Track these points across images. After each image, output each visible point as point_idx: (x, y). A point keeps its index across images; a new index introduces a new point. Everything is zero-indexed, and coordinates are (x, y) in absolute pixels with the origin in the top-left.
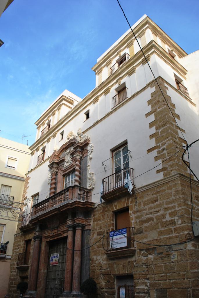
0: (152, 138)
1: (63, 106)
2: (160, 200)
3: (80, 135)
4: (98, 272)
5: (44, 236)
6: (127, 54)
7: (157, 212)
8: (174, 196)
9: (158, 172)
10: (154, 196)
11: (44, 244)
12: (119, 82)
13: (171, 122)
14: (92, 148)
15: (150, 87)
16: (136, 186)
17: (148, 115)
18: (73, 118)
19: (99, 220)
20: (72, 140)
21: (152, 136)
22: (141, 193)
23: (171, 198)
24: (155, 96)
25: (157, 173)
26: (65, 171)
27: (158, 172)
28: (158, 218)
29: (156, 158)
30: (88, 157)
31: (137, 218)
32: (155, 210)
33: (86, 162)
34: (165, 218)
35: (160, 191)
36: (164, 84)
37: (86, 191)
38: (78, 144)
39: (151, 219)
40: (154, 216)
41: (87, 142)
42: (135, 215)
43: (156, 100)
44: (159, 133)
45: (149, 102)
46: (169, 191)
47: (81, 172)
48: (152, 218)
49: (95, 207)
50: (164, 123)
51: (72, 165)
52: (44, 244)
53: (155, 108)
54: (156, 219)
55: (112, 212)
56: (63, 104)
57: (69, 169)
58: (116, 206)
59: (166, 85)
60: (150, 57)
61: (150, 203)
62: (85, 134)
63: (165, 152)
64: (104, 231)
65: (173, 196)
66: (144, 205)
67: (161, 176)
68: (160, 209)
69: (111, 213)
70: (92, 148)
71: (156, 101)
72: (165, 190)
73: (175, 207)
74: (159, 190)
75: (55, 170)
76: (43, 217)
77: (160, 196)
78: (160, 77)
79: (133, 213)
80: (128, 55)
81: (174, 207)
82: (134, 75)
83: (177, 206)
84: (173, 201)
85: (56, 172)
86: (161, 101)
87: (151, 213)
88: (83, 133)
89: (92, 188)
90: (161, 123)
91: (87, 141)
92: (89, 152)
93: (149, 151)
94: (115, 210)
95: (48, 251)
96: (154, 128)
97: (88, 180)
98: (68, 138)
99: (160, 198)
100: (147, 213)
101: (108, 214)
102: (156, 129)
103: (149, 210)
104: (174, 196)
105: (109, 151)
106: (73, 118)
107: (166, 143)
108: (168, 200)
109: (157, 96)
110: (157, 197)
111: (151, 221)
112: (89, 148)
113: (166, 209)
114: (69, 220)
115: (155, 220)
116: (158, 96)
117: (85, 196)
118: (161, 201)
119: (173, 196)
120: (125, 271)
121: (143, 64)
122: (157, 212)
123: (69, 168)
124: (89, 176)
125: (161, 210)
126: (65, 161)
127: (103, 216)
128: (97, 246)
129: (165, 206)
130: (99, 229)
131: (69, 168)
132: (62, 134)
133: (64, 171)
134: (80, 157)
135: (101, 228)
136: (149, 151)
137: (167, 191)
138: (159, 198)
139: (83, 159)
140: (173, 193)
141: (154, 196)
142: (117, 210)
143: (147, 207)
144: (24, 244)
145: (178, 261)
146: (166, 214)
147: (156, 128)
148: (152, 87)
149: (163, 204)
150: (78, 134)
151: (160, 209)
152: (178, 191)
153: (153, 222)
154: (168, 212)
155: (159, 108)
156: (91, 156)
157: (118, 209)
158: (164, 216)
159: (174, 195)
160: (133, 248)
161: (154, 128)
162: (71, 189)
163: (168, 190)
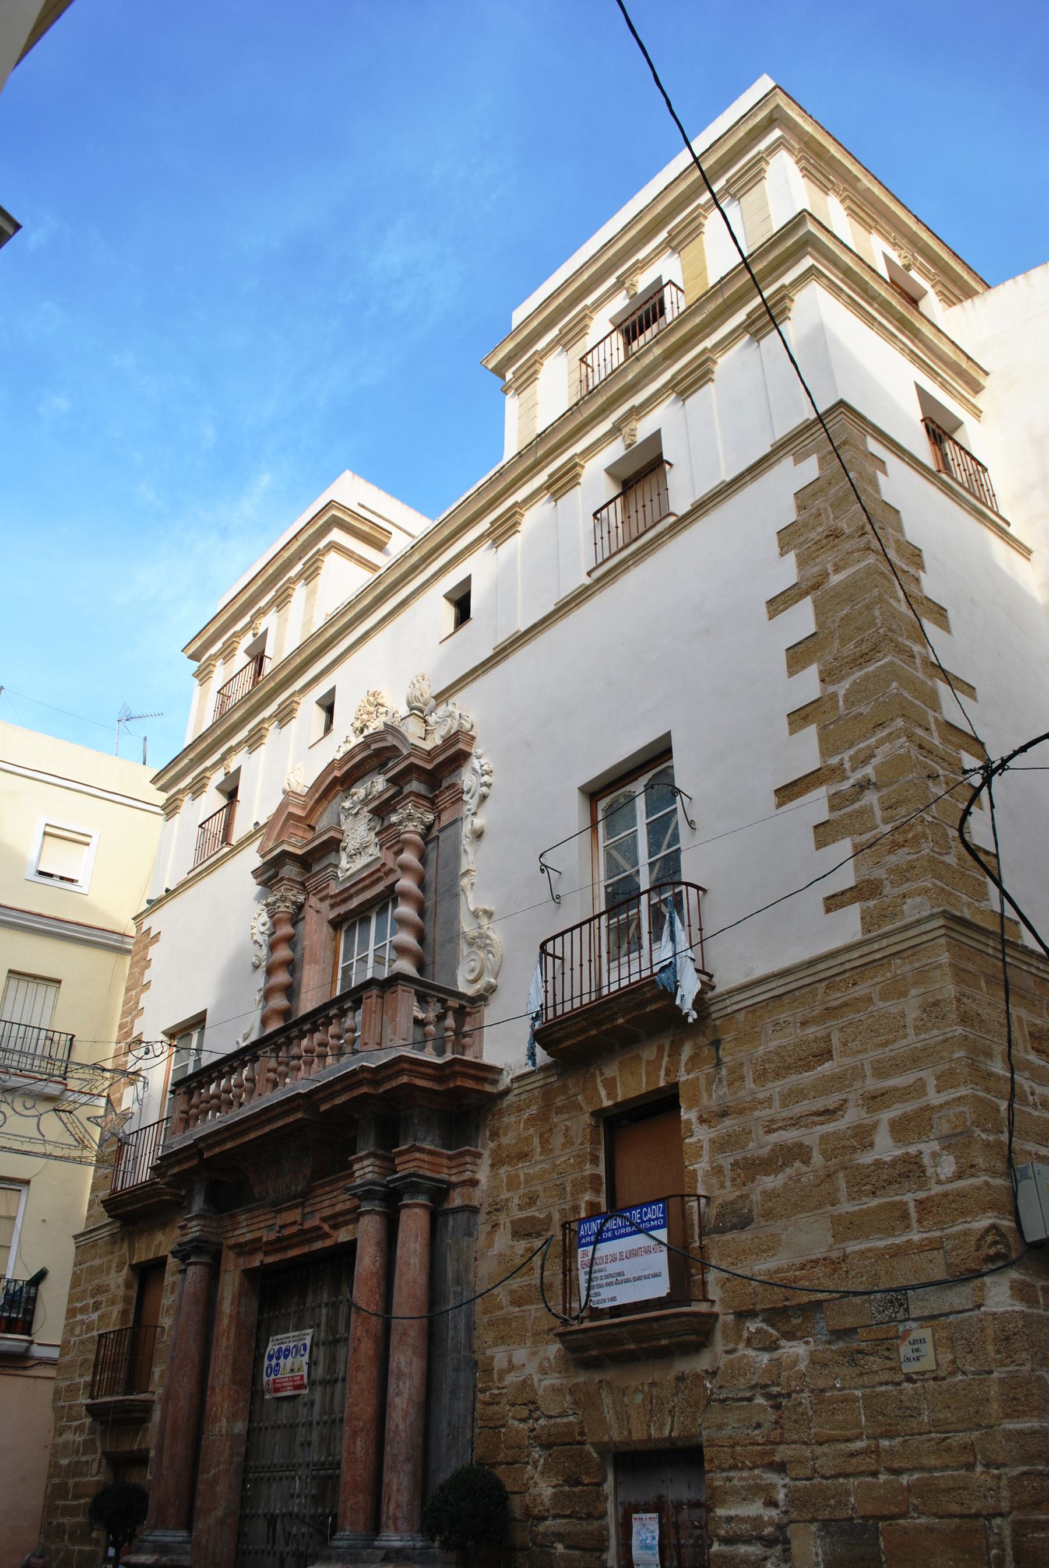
0: (802, 727)
3: (422, 712)
5: (232, 1241)
6: (670, 282)
7: (829, 1113)
9: (834, 902)
10: (811, 1031)
12: (626, 430)
13: (900, 639)
14: (486, 778)
17: (778, 604)
19: (523, 1156)
20: (377, 736)
21: (799, 718)
22: (741, 1016)
23: (904, 1042)
24: (819, 503)
25: (828, 910)
26: (345, 901)
27: (834, 902)
28: (833, 1147)
30: (466, 828)
31: (721, 1145)
32: (820, 1104)
34: (872, 1145)
37: (453, 1003)
38: (410, 755)
39: (799, 1153)
40: (811, 1136)
44: (841, 703)
45: (787, 538)
46: (892, 1007)
47: (429, 904)
48: (800, 1145)
49: (501, 1087)
50: (864, 648)
51: (378, 870)
53: (818, 568)
54: (823, 1152)
55: (593, 1114)
56: (333, 546)
58: (610, 1085)
59: (874, 446)
60: (792, 300)
61: (788, 1068)
62: (450, 708)
64: (549, 1217)
65: (911, 1031)
66: (762, 1077)
69: (586, 1118)
72: (869, 1000)
73: (924, 1087)
74: (837, 998)
77: (841, 1030)
79: (702, 1120)
80: (674, 289)
81: (918, 1089)
83: (931, 1083)
84: (915, 1059)
85: (294, 903)
86: (847, 531)
87: (795, 1122)
88: (436, 698)
90: (851, 646)
91: (457, 742)
93: (787, 793)
94: (607, 1103)
97: (464, 949)
98: (358, 724)
99: (845, 1044)
102: (822, 681)
103: (784, 1105)
107: (876, 751)
110: (828, 1038)
111: (797, 1164)
112: (467, 779)
113: (875, 1100)
114: (361, 1159)
115: (817, 1159)
116: (832, 505)
117: (446, 1030)
118: (846, 1060)
119: (911, 1031)
120: (661, 1428)
122: (829, 1113)
125: (850, 1104)
127: (541, 1135)
128: (512, 1292)
129: (872, 1084)
130: (521, 1207)
133: (338, 899)
136: (787, 793)
137: (881, 1004)
138: (835, 1042)
143: (776, 1087)
144: (128, 1285)
145: (941, 1374)
146: (874, 1127)
147: (821, 672)
149: (857, 1073)
150: (409, 703)
153: (804, 1169)
154: (886, 1116)
155: (837, 569)
156: (478, 822)
158: (863, 1136)
159: (916, 1028)
160: (703, 1307)
163: (885, 996)
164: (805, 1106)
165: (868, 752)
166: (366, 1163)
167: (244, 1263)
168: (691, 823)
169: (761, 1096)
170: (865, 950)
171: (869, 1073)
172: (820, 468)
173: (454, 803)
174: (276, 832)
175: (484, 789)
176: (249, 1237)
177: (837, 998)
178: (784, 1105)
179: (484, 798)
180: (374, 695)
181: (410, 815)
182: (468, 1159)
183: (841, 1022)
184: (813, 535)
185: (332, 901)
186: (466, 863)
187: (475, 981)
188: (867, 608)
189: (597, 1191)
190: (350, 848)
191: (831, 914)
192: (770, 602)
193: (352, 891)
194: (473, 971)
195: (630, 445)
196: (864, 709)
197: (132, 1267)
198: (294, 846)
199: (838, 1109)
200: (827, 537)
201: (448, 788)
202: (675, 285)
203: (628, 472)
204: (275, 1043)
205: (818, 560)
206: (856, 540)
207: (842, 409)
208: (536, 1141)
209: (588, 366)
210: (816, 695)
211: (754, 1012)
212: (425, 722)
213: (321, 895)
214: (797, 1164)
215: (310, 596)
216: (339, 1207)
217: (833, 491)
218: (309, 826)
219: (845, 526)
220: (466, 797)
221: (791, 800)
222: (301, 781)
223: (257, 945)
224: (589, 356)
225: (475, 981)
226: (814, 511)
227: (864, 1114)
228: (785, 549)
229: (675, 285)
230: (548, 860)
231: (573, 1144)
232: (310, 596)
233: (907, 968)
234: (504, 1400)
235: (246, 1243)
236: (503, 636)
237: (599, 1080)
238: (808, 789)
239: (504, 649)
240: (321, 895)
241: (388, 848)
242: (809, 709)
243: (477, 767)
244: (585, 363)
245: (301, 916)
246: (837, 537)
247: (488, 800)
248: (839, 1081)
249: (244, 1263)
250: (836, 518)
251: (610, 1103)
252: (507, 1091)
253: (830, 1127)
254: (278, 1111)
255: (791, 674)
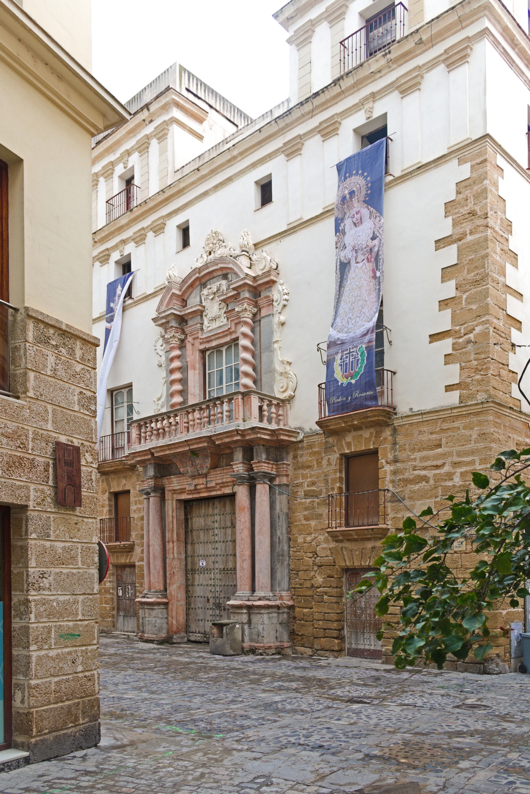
0: (445, 309)
1: (175, 129)
2: (446, 447)
3: (248, 253)
4: (308, 561)
5: (171, 488)
6: (401, 3)
7: (437, 467)
8: (475, 442)
9: (449, 388)
10: (434, 436)
11: (171, 506)
12: (366, 107)
13: (494, 275)
14: (286, 297)
15: (457, 161)
16: (397, 410)
17: (440, 243)
18: (216, 188)
19: (309, 467)
20: (222, 259)
21: (444, 304)
22: (407, 426)
23: (470, 446)
24: (467, 193)
25: (446, 391)
26: (208, 342)
27: (449, 388)
28: (438, 479)
29: (448, 359)
30: (276, 319)
31: (395, 473)
32: (435, 463)
33: (271, 333)
34: (452, 479)
35: (447, 429)
36: (495, 158)
37: (275, 402)
38: (245, 278)
39: (425, 479)
40: (430, 473)
41: (273, 278)
42: (392, 468)
43: (467, 205)
44: (464, 302)
45: (449, 207)
46: (467, 432)
47: (257, 352)
48: (426, 476)
49: (299, 439)
50: (478, 278)
51: (227, 331)
52: (171, 506)
53: (462, 230)
54: (434, 480)
55: (340, 454)
56: (174, 120)
57: (219, 338)
58: (349, 445)
59: (501, 161)
60: (471, 49)
61: (424, 449)
62: (264, 254)
63: (470, 347)
64: (321, 490)
65: (472, 442)
66: (413, 450)
67: (454, 398)
68: (445, 463)
69: (338, 455)
70: (286, 297)
71: (466, 208)
72: (458, 428)
73: (475, 462)
74: (445, 426)
75: (177, 335)
76: (166, 450)
77: (446, 438)
78: (487, 136)
79: (387, 463)
80: (402, 8)
81: (473, 462)
82: (414, 98)
83: (478, 462)
84: (472, 453)
85: (179, 339)
86: (479, 213)
87: (425, 468)
88: (255, 245)
89: (289, 397)
90: (472, 274)
91: (270, 275)
92: (277, 307)
93: (434, 337)
94: (347, 451)
95: (183, 517)
96: (452, 283)
97: (278, 377)
98: (208, 249)
99: (447, 443)
100: (415, 467)
101: (329, 459)
102: (457, 289)
103: (421, 462)
104: (475, 442)
105: (253, 184)
106: (216, 188)
107: (476, 328)
108: (460, 448)
109: (471, 195)
110: (441, 440)
111: (424, 482)
112: (275, 294)
113: (455, 464)
114: (236, 464)
115: (432, 482)
116: (473, 196)
117: (272, 413)
118: (446, 449)
119: (472, 442)
120: (365, 562)
121: (448, 66)
122: (437, 467)
123: (217, 336)
124: (279, 368)
125: (447, 464)
126: (206, 316)
127: (317, 460)
128: (304, 515)
129: (456, 459)
130: (308, 486)
131: (217, 336)
132: (185, 231)
133: (205, 340)
134: (251, 316)
135: (313, 484)
136: (434, 337)
137: (463, 431)
138: (444, 441)
139: (260, 321)
140: (475, 436)
141: (435, 436)
142: (351, 452)
143: (418, 455)
144: (110, 500)
145: (467, 551)
146: (454, 473)
147: (457, 284)
148: (461, 162)
149: (450, 454)
150: (241, 247)
151: (445, 463)
152: (484, 434)
153: (426, 484)
154: (459, 470)
155: (471, 233)
156: (282, 318)
157: (353, 450)
158: (450, 476)
159: (475, 441)
160: (384, 526)
161: (452, 283)
162: (240, 397)
163: (465, 428)
164: (429, 463)
165: (472, 327)
166: (239, 466)
167: (177, 497)
168: (390, 342)
169: (412, 457)
170: (460, 410)
171: (455, 454)
172: (471, 172)
173: (268, 305)
174: (166, 302)
175: (285, 302)
176: (179, 487)
177: (445, 426)
178: (421, 462)
179: (285, 306)
180: (215, 233)
181: (246, 309)
182: (285, 466)
183: (446, 435)
184: (462, 210)
185: (201, 341)
186: (276, 338)
187: (284, 392)
188: (482, 258)
189: (342, 483)
190: (209, 316)
191: (448, 393)
192: (437, 242)
193: (212, 338)
194: (282, 387)
195: (369, 118)
196: (474, 307)
197: (110, 493)
198: (177, 310)
199: (440, 466)
200: (469, 213)
201: (265, 297)
202: (404, 6)
203: (366, 132)
204: (187, 411)
205: (463, 225)
206: (483, 220)
207: (488, 140)
208: (315, 462)
209: (345, 47)
210: (453, 295)
211: (412, 426)
212: (250, 259)
213: (194, 337)
214: (424, 482)
215: (163, 152)
216: (225, 480)
217: (475, 188)
218: (183, 300)
219: (478, 211)
220: (275, 304)
221: (436, 341)
222: (176, 274)
223: (158, 356)
224: (346, 41)
225: (284, 392)
226: (464, 196)
227: (451, 469)
228: (448, 214)
229: (404, 6)
230: (320, 346)
231: (331, 465)
232: (163, 152)
233: (475, 419)
234: (302, 551)
235: (177, 490)
236: (294, 218)
237: (343, 442)
238: (443, 338)
239: (294, 228)
240: (194, 337)
241: (231, 321)
242: (449, 301)
243: (281, 290)
244: (343, 45)
245: (184, 345)
246: (473, 215)
247: (287, 307)
248: (444, 455)
249: (177, 497)
250: (475, 204)
251: (349, 451)
252: (301, 441)
253: (437, 471)
254: (194, 441)
255: (442, 282)
